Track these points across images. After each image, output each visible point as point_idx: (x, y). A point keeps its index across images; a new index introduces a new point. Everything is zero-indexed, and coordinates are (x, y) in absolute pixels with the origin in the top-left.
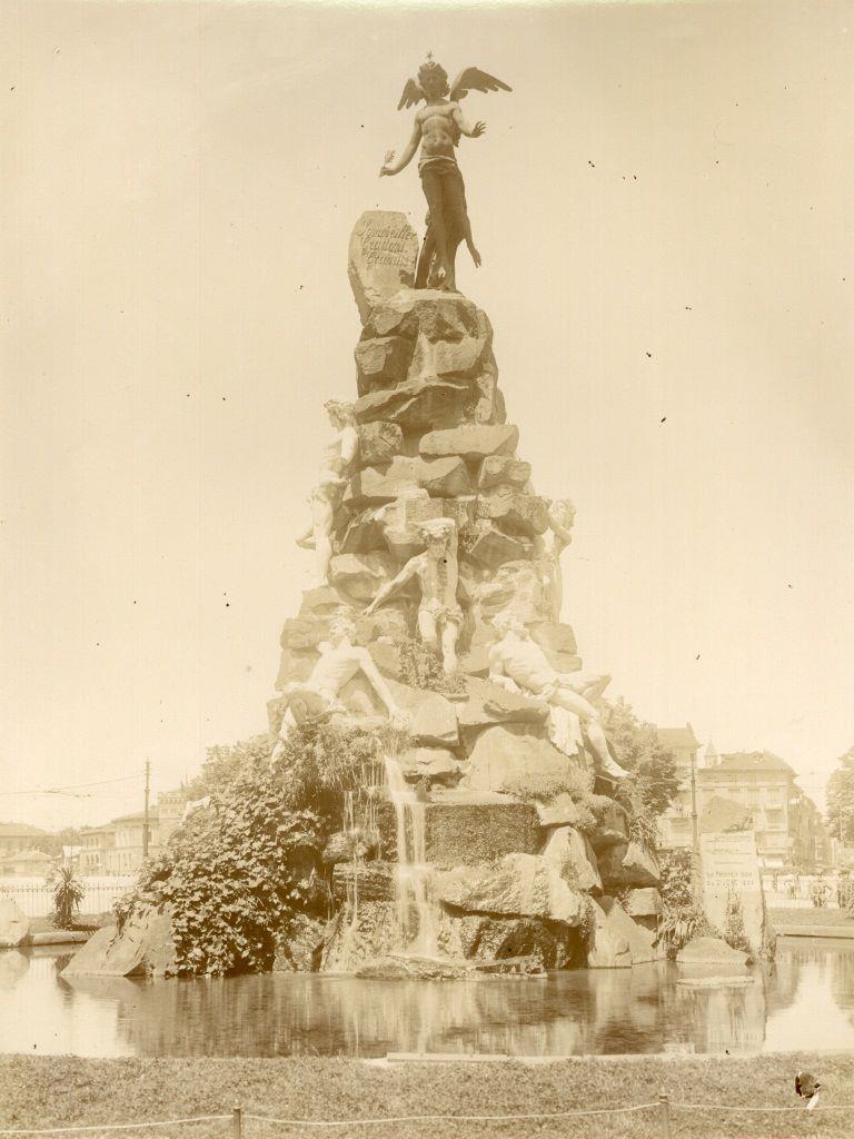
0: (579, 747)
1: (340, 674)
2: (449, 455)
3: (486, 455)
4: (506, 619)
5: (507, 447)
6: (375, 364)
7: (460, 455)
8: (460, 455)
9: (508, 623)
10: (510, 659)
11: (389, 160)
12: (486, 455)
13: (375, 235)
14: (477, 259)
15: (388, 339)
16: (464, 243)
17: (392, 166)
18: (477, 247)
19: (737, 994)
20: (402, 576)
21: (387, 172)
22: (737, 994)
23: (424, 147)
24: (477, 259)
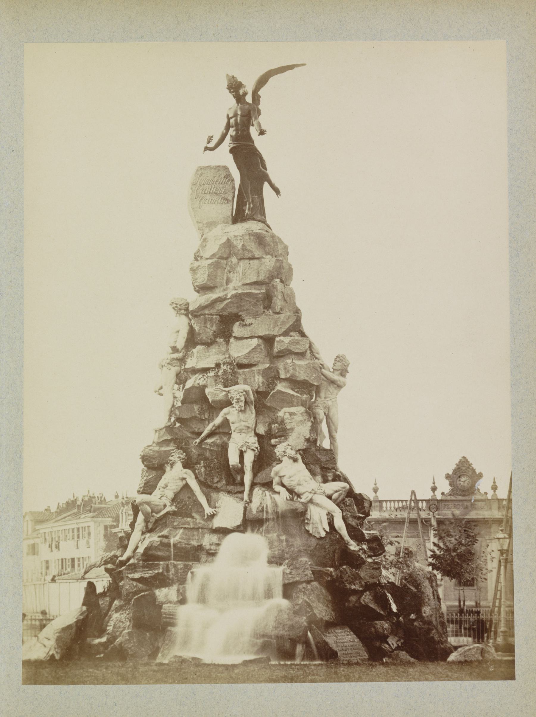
0: (327, 532)
1: (175, 491)
2: (252, 337)
3: (276, 336)
4: (283, 450)
5: (296, 327)
6: (202, 278)
7: (259, 337)
8: (259, 337)
9: (284, 452)
10: (283, 476)
11: (209, 142)
12: (276, 336)
13: (206, 184)
14: (277, 191)
15: (210, 261)
16: (266, 185)
17: (212, 145)
18: (277, 185)
19: (27, 582)
20: (218, 421)
21: (206, 149)
22: (27, 582)
23: (231, 136)
24: (277, 191)
